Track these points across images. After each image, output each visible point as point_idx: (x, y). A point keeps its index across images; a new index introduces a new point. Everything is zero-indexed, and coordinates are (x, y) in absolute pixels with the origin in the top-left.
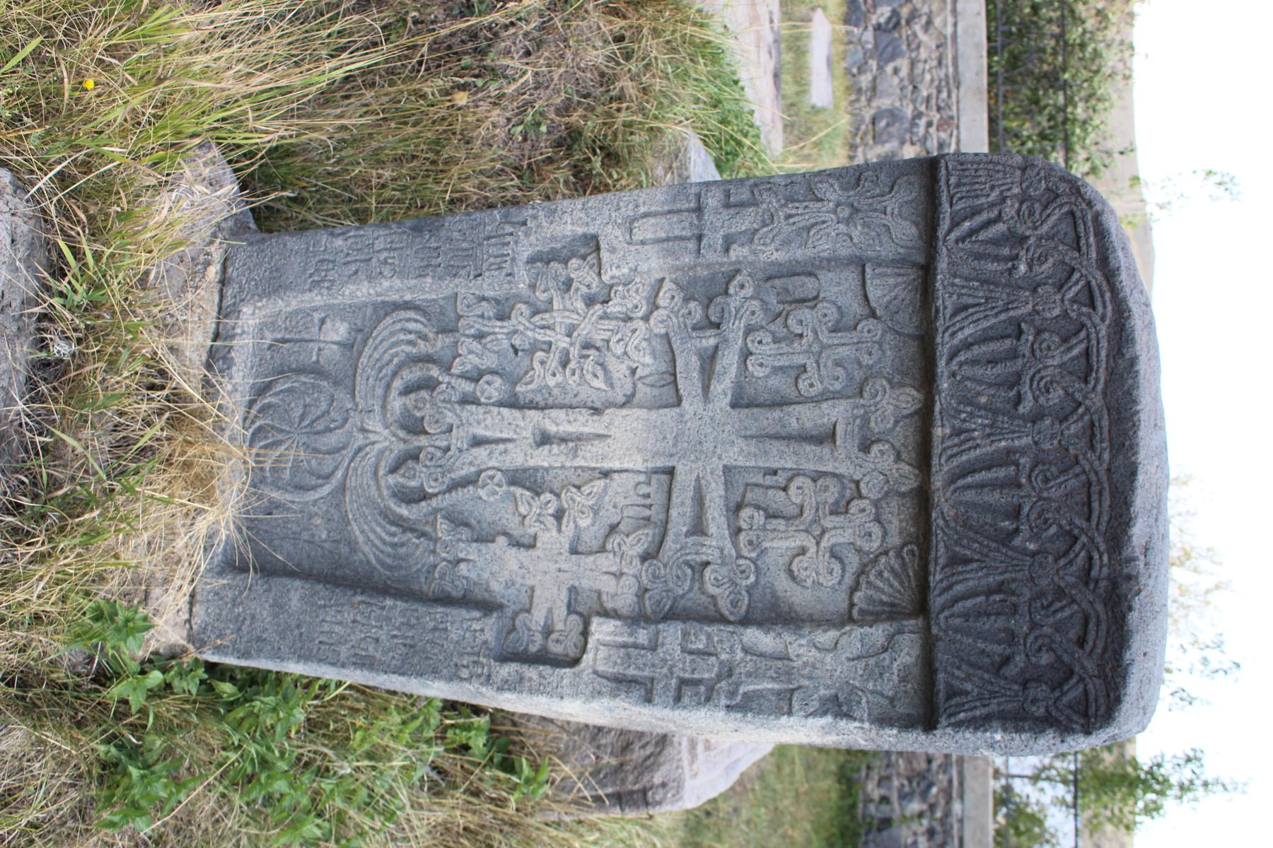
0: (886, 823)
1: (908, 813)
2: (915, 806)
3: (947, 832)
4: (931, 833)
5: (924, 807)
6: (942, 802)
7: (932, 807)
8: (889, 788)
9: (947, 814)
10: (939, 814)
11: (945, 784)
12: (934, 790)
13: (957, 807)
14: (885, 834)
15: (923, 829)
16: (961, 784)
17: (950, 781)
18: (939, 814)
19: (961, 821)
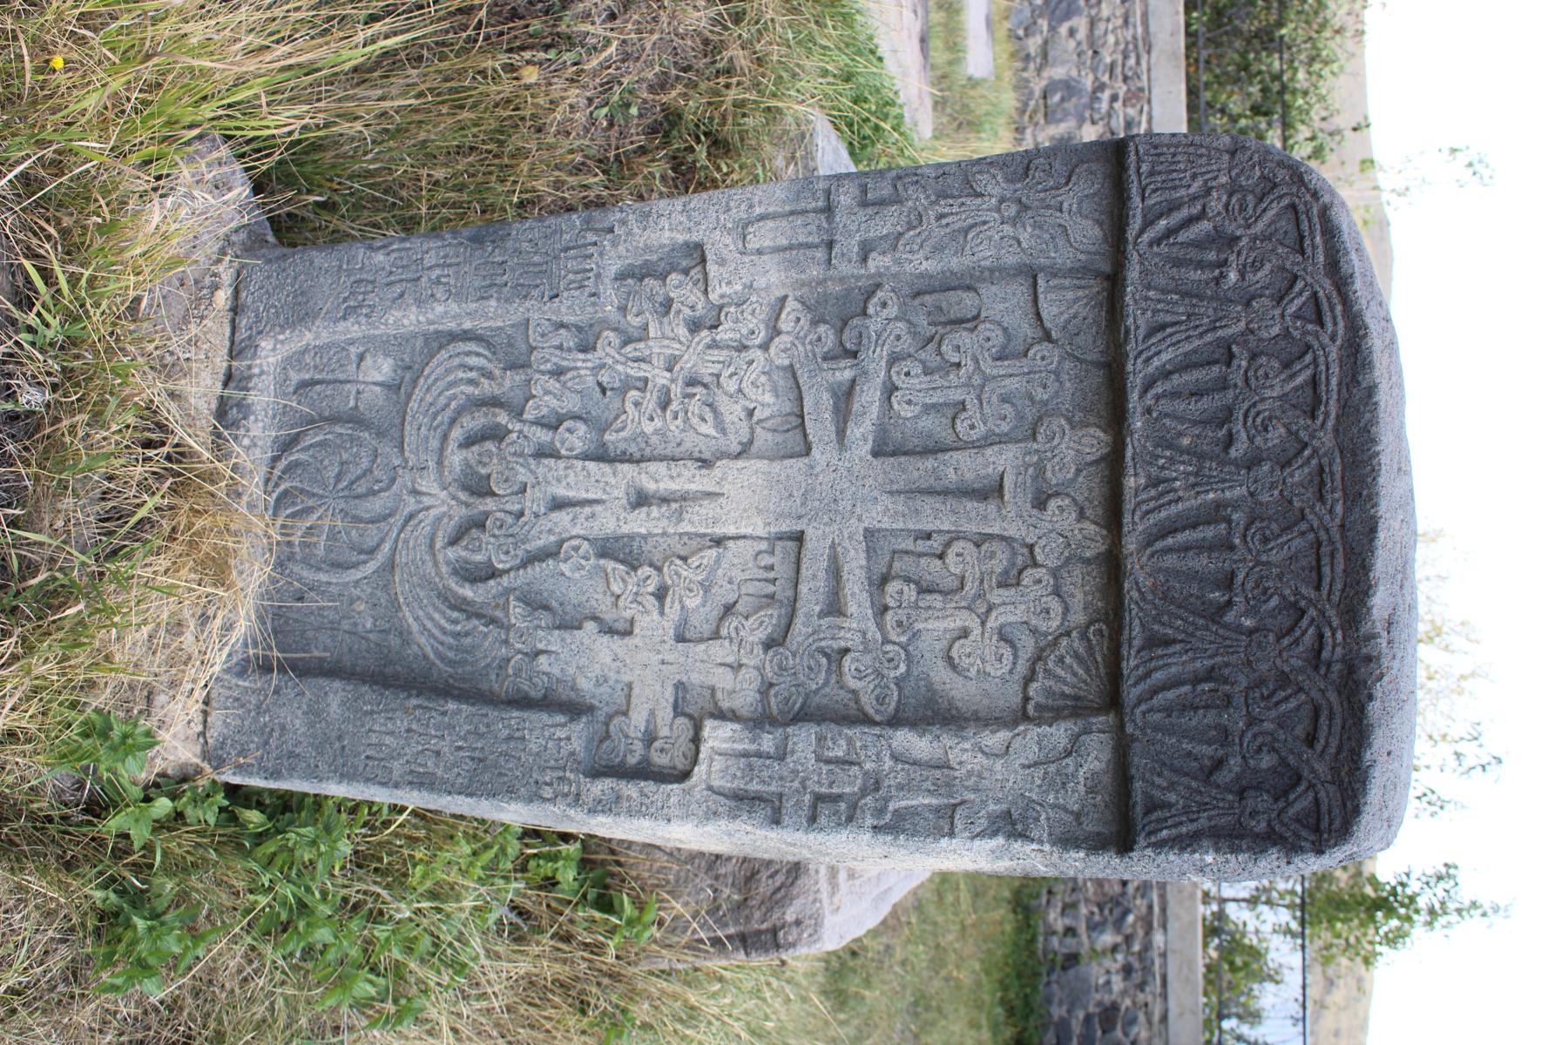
0: (1072, 959)
1: (1099, 947)
2: (1108, 938)
3: (1147, 970)
4: (1127, 970)
5: (1119, 939)
6: (1141, 932)
7: (1128, 939)
8: (1076, 917)
9: (1147, 947)
10: (1136, 948)
11: (1144, 910)
12: (1131, 918)
13: (1158, 938)
14: (1071, 972)
15: (1118, 966)
16: (1164, 910)
17: (1150, 907)
18: (1136, 948)
19: (1164, 955)
